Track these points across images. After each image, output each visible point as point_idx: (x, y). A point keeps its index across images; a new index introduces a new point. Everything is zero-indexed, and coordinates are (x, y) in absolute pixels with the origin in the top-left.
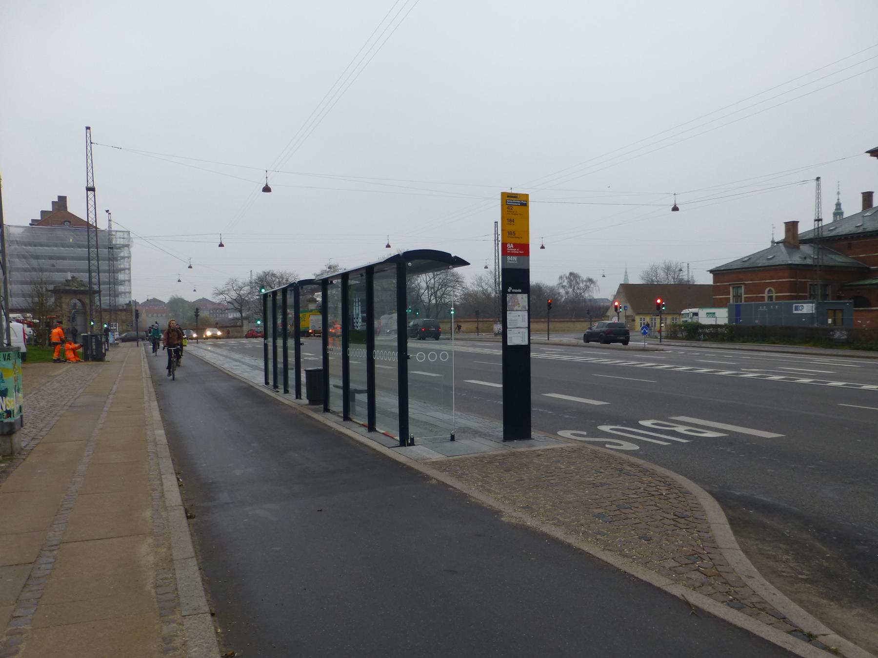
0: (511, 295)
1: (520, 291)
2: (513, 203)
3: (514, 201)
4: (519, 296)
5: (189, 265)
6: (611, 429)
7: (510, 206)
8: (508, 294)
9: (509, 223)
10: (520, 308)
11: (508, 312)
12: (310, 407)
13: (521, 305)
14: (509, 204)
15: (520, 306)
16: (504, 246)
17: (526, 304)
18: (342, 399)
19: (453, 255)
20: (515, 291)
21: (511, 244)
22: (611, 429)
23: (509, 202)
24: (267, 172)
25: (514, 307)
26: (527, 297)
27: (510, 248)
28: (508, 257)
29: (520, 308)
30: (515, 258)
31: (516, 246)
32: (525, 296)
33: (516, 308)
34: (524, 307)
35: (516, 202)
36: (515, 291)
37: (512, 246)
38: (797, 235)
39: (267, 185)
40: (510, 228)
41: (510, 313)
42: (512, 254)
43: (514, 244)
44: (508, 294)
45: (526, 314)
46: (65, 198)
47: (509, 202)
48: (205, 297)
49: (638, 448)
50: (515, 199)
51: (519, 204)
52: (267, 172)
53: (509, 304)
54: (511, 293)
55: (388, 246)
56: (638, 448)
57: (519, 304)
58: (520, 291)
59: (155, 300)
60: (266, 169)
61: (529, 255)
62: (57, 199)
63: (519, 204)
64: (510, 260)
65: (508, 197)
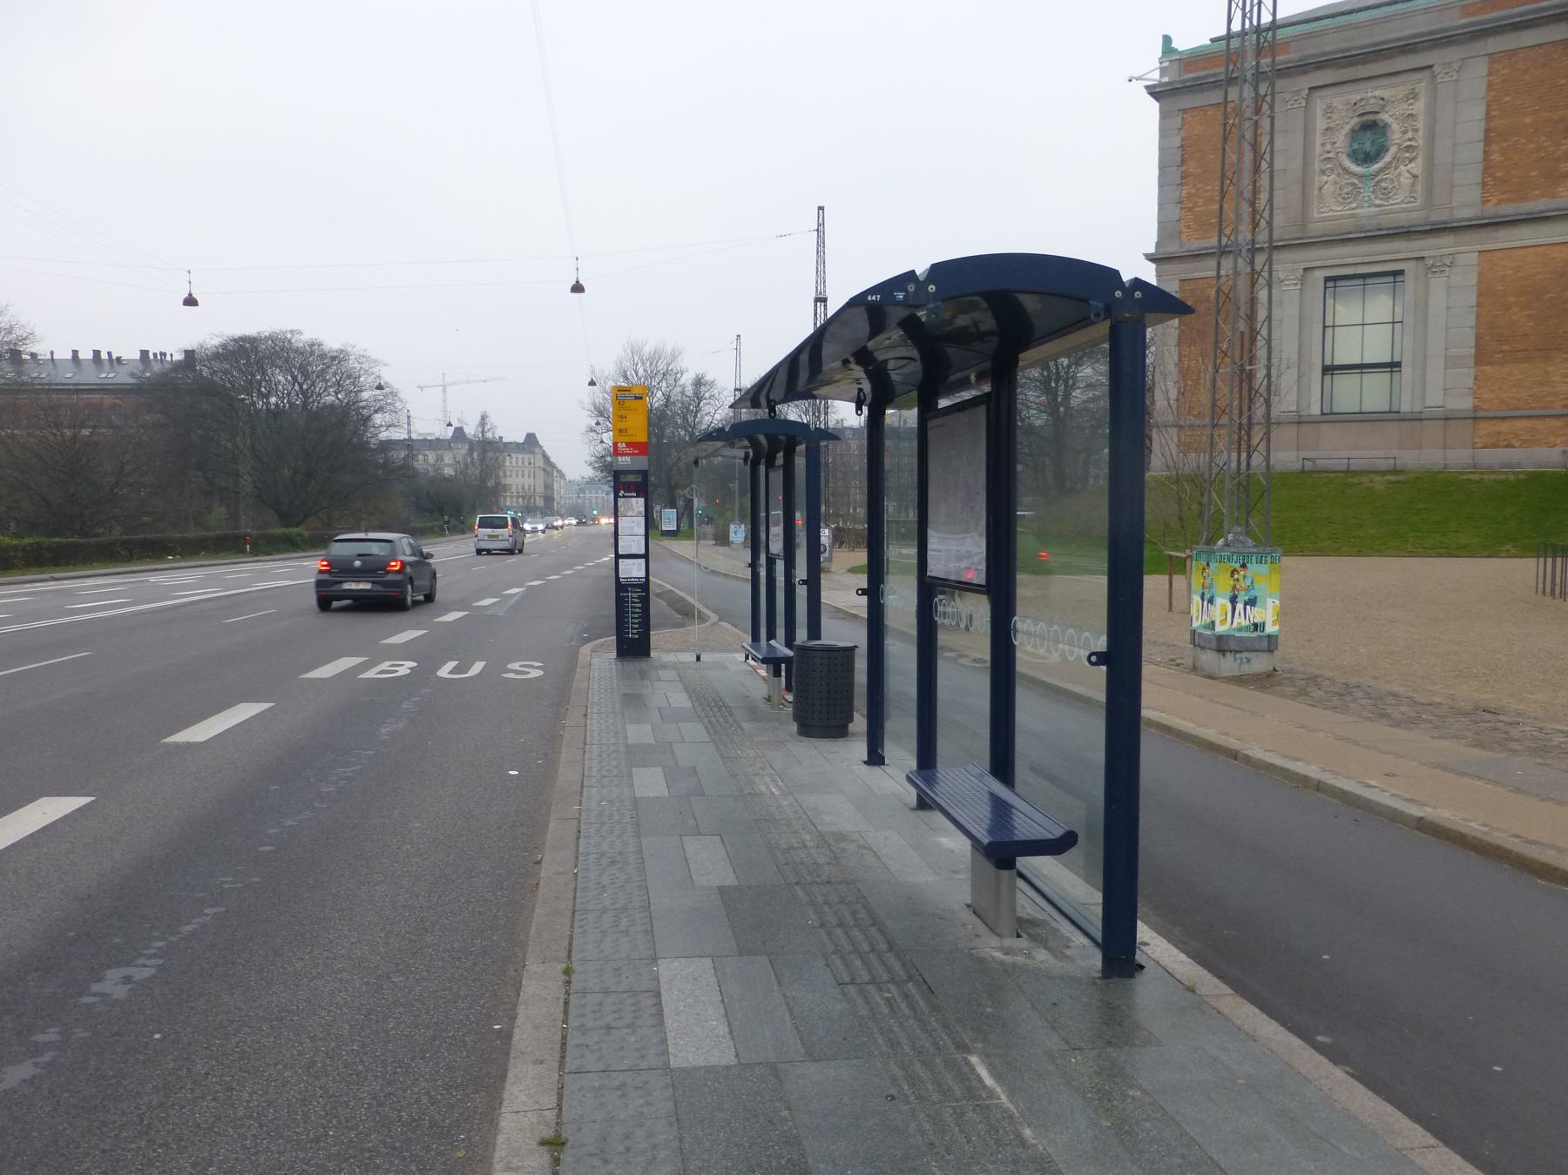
6: (528, 673)
12: (1188, 573)
17: (642, 509)
18: (1107, 559)
19: (1126, 277)
20: (629, 494)
22: (528, 673)
24: (577, 259)
28: (620, 458)
30: (628, 459)
31: (629, 445)
32: (641, 500)
33: (630, 513)
36: (629, 494)
37: (624, 445)
38: (992, 383)
39: (577, 282)
40: (621, 425)
42: (623, 454)
45: (642, 520)
46: (197, 305)
48: (537, 436)
52: (577, 259)
53: (621, 509)
54: (624, 496)
59: (934, 266)
62: (139, 355)
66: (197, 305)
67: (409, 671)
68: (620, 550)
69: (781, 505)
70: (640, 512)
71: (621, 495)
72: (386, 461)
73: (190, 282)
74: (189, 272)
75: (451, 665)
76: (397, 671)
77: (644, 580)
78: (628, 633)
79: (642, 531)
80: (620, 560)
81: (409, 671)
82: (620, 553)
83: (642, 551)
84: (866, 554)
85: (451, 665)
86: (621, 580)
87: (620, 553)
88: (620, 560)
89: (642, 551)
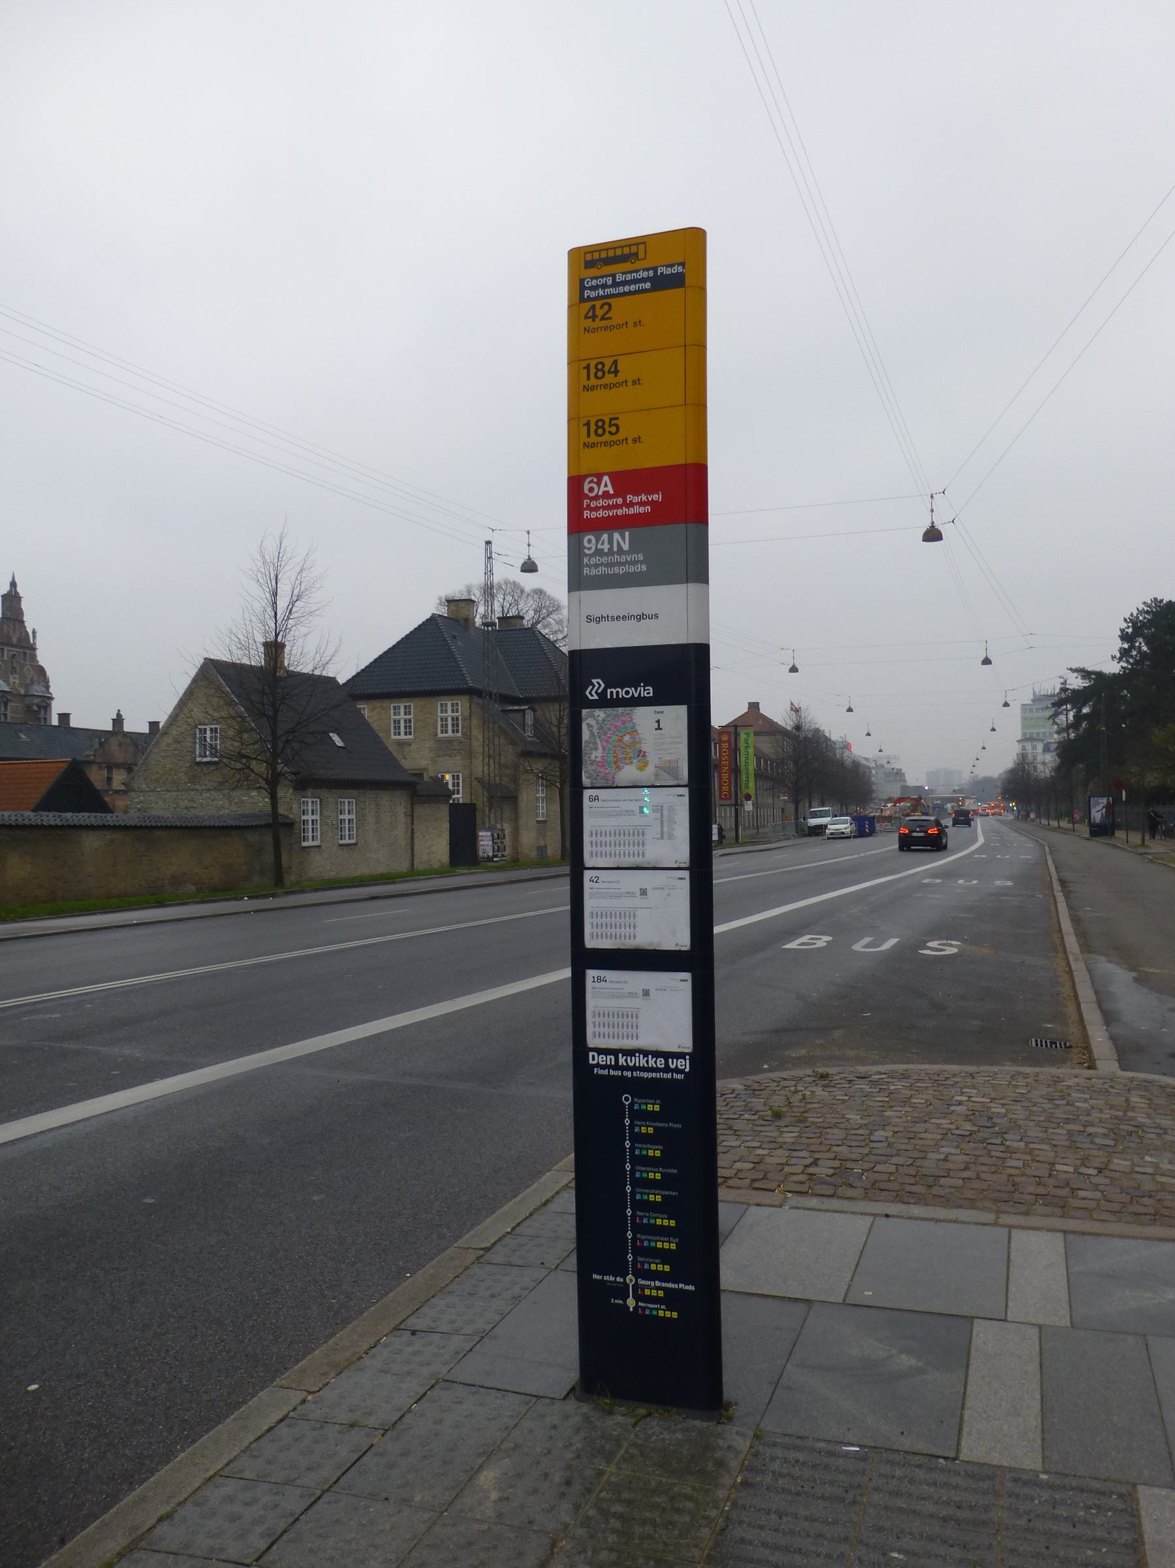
0: (600, 714)
1: (649, 692)
2: (615, 284)
3: (619, 278)
4: (644, 716)
5: (848, 707)
7: (598, 304)
8: (584, 712)
9: (594, 381)
10: (650, 769)
11: (587, 794)
13: (653, 759)
14: (593, 294)
15: (646, 764)
16: (575, 485)
21: (599, 476)
23: (593, 288)
25: (619, 768)
26: (668, 945)
27: (597, 498)
29: (648, 775)
31: (626, 482)
33: (629, 773)
34: (670, 769)
35: (629, 277)
37: (607, 485)
40: (603, 403)
41: (597, 798)
43: (615, 477)
44: (584, 712)
45: (679, 803)
46: (536, 570)
47: (593, 288)
49: (853, 947)
50: (626, 266)
51: (648, 285)
52: (528, 533)
53: (594, 755)
54: (603, 702)
55: (881, 751)
56: (853, 947)
57: (641, 754)
58: (649, 692)
60: (526, 530)
61: (707, 524)
63: (648, 285)
64: (599, 552)
65: (589, 264)
66: (536, 570)
67: (825, 944)
68: (588, 929)
69: (717, 944)
70: (671, 770)
71: (592, 694)
72: (905, 788)
73: (529, 545)
74: (528, 533)
75: (867, 940)
76: (815, 944)
77: (684, 1065)
78: (623, 1292)
79: (679, 849)
80: (591, 974)
81: (825, 944)
82: (590, 943)
83: (679, 938)
84: (781, 723)
85: (867, 940)
86: (594, 1059)
87: (590, 943)
88: (591, 974)
89: (679, 938)
